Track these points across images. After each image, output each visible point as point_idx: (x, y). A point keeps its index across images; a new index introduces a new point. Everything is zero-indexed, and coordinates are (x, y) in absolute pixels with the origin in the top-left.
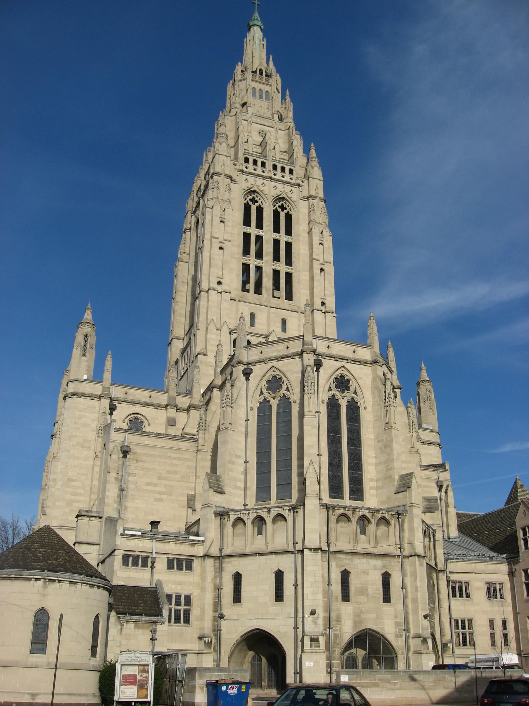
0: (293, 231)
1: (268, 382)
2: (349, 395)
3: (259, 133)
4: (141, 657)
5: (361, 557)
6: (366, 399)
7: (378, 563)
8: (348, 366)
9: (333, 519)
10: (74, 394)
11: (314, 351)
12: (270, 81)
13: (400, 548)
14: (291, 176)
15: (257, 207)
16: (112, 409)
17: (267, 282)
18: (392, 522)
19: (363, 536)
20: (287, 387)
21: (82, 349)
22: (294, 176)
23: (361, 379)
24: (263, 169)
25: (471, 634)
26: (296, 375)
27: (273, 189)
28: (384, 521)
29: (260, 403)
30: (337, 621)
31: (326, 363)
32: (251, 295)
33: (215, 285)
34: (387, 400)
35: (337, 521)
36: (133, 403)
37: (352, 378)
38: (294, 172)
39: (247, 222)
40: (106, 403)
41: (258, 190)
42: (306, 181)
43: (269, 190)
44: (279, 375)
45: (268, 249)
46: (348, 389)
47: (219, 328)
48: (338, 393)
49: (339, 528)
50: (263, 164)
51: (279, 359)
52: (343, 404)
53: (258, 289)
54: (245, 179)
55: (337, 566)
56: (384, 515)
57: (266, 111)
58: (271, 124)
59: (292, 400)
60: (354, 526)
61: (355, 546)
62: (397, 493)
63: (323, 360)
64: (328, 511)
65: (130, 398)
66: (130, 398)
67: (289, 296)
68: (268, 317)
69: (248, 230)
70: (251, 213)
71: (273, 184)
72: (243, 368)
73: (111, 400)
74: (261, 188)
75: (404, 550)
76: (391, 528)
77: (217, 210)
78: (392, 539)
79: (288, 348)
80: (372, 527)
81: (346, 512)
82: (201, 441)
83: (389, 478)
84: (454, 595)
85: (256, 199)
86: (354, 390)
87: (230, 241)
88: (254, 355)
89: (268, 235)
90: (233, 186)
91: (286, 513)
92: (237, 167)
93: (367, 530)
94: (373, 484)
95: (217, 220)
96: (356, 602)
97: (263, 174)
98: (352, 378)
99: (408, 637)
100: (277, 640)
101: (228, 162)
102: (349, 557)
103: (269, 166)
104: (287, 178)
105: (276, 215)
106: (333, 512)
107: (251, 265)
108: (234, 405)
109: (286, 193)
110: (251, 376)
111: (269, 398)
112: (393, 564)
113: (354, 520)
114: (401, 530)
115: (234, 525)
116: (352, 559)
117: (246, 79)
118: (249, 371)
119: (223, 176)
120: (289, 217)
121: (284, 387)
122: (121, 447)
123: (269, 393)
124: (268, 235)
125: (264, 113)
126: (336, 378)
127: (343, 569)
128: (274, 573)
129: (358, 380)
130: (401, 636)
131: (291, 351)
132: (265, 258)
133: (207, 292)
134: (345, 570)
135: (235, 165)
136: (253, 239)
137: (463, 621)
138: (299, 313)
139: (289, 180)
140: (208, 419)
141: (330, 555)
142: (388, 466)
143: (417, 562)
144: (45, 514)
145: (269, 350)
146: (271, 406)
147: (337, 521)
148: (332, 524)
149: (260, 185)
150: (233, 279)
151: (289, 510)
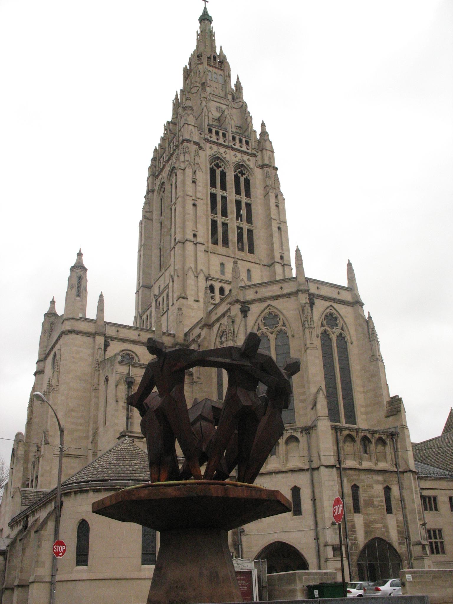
0: (252, 194)
1: (265, 318)
2: (338, 331)
3: (217, 109)
4: (242, 564)
5: (366, 473)
6: (351, 335)
7: (380, 478)
8: (336, 306)
9: (341, 439)
11: (105, 335)
12: (223, 66)
13: (396, 465)
15: (221, 172)
16: (106, 345)
17: (233, 237)
18: (388, 442)
19: (365, 455)
21: (82, 287)
23: (346, 317)
25: (442, 543)
26: (291, 312)
27: (233, 158)
28: (381, 441)
30: (351, 531)
31: (317, 302)
32: (220, 248)
33: (190, 237)
34: (371, 335)
35: (345, 441)
36: (123, 340)
37: (339, 316)
38: (250, 144)
39: (213, 184)
40: (100, 340)
41: (221, 157)
42: (260, 152)
43: (232, 158)
44: (275, 312)
45: (232, 207)
46: (336, 325)
47: (196, 275)
48: (329, 329)
49: (346, 447)
50: (224, 135)
52: (334, 338)
53: (226, 243)
55: (348, 481)
56: (380, 436)
57: (221, 91)
58: (226, 103)
60: (358, 445)
61: (360, 464)
62: (387, 417)
64: (336, 433)
65: (121, 335)
67: (251, 250)
69: (214, 191)
71: (233, 153)
72: (240, 307)
73: (106, 337)
74: (224, 155)
75: (399, 467)
76: (388, 448)
77: (189, 172)
78: (389, 457)
80: (372, 446)
81: (351, 433)
83: (379, 404)
84: (426, 509)
87: (202, 199)
88: (250, 295)
89: (232, 196)
90: (200, 152)
91: (298, 435)
92: (202, 136)
93: (368, 449)
94: (362, 410)
95: (189, 182)
96: (365, 514)
97: (225, 144)
98: (339, 316)
99: (410, 544)
100: (298, 551)
101: (196, 132)
102: (357, 473)
103: (229, 136)
104: (244, 149)
105: (237, 179)
106: (341, 433)
107: (218, 222)
108: (236, 339)
109: (245, 162)
110: (249, 314)
111: (268, 333)
112: (391, 479)
113: (358, 439)
114: (396, 450)
115: (287, 442)
116: (359, 475)
117: (202, 63)
118: (246, 309)
119: (192, 143)
120: (247, 181)
121: (281, 323)
122: (126, 379)
123: (267, 329)
124: (232, 196)
125: (219, 93)
126: (326, 316)
127: (353, 484)
128: (291, 489)
129: (344, 318)
130: (403, 544)
132: (230, 216)
133: (183, 243)
134: (355, 485)
135: (201, 134)
136: (219, 199)
137: (434, 532)
139: (246, 150)
141: (342, 472)
142: (376, 393)
143: (412, 476)
144: (47, 443)
145: (264, 290)
146: (269, 340)
147: (345, 441)
148: (341, 445)
150: (204, 232)
151: (302, 432)
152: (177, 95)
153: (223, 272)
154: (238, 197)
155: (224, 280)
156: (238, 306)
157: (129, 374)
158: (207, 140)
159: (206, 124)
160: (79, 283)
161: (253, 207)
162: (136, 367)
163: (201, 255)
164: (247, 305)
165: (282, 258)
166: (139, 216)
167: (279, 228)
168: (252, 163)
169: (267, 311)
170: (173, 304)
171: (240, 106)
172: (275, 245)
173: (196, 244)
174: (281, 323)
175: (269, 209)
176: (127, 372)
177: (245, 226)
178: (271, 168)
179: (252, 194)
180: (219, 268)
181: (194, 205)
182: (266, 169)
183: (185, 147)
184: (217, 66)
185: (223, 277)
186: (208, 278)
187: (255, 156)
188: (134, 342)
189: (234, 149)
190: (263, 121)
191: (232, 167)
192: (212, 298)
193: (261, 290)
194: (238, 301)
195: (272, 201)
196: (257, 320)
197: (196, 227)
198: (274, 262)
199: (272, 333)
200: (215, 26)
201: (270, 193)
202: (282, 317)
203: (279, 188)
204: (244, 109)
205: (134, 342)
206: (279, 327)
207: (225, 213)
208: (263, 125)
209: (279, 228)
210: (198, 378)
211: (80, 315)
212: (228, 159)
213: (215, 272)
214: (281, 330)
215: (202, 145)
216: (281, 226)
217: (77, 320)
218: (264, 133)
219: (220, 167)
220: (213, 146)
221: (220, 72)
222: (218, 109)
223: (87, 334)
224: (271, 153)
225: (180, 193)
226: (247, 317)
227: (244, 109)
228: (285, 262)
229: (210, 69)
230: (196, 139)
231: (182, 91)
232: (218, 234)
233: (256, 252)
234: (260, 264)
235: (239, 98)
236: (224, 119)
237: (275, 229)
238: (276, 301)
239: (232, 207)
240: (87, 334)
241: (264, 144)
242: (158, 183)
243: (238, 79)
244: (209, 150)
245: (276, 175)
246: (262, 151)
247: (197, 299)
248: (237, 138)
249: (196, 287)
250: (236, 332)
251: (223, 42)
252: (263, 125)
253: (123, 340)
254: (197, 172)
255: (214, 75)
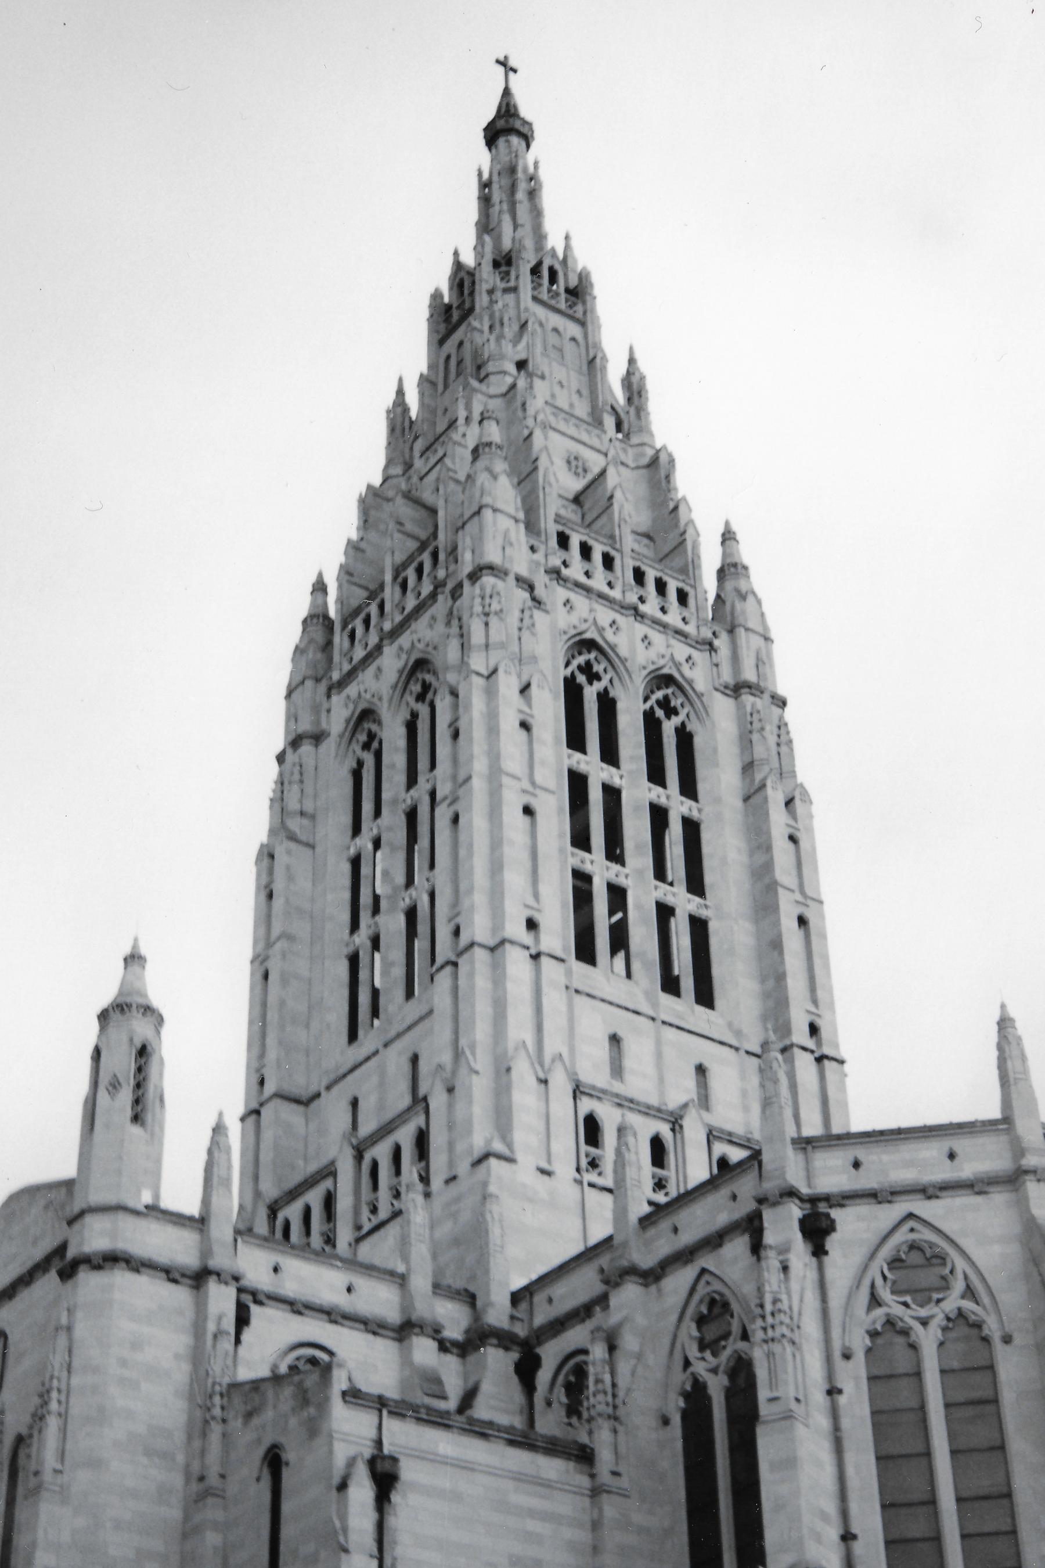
3: (569, 462)
10: (112, 1259)
14: (686, 614)
16: (242, 1319)
20: (968, 1287)
22: (690, 612)
24: (610, 576)
27: (640, 646)
29: (873, 1334)
33: (516, 929)
40: (222, 1300)
43: (640, 648)
44: (932, 1245)
45: (636, 829)
47: (542, 1076)
50: (608, 562)
51: (928, 1192)
54: (563, 600)
58: (595, 442)
59: (992, 1327)
63: (829, 1210)
66: (289, 1288)
67: (705, 996)
68: (659, 1055)
70: (585, 714)
73: (240, 1290)
79: (952, 1156)
82: (605, 1457)
85: (598, 668)
86: (740, 1331)
88: (831, 1174)
89: (638, 793)
90: (538, 614)
95: (509, 722)
101: (519, 535)
110: (832, 1242)
111: (907, 1319)
119: (511, 579)
123: (906, 1304)
124: (638, 793)
131: (967, 1169)
135: (532, 549)
138: (742, 1052)
140: (622, 1382)
145: (885, 1158)
149: (606, 625)
152: (400, 392)
153: (617, 1070)
154: (656, 794)
155: (631, 1101)
156: (795, 1211)
157: (379, 1443)
158: (555, 574)
159: (551, 517)
160: (139, 1070)
161: (706, 836)
162: (403, 1416)
163: (554, 1000)
164: (822, 1207)
165: (814, 1030)
166: (256, 826)
167: (802, 921)
168: (699, 675)
169: (902, 1236)
170: (452, 1179)
171: (645, 461)
172: (790, 982)
173: (536, 957)
174: (959, 1286)
175: (766, 847)
176: (373, 1433)
177: (684, 903)
178: (766, 696)
179: (702, 787)
180: (602, 1051)
181: (528, 811)
182: (748, 699)
183: (488, 591)
184: (563, 306)
185: (617, 1087)
186: (578, 1091)
187: (712, 648)
188: (332, 1315)
189: (639, 615)
190: (727, 524)
191: (639, 683)
192: (593, 1164)
193: (874, 1158)
194: (791, 1193)
195: (778, 820)
196: (865, 1268)
197: (536, 896)
198: (792, 1045)
199: (924, 1322)
200: (545, 155)
201: (769, 790)
202: (960, 1264)
203: (793, 774)
204: (663, 473)
205: (332, 1315)
206: (953, 1302)
207: (615, 852)
208: (728, 537)
209: (802, 921)
210: (615, 1474)
211: (147, 1198)
212: (623, 651)
213: (593, 1068)
214: (961, 1313)
215: (540, 591)
216: (809, 915)
217: (136, 1213)
218: (730, 570)
219: (598, 678)
220: (573, 596)
221: (573, 329)
222: (575, 464)
223: (170, 1274)
224: (761, 642)
225: (480, 766)
226: (826, 1253)
227: (663, 473)
228: (827, 1050)
229: (540, 312)
230: (524, 572)
231: (426, 382)
232: (594, 931)
233: (718, 1002)
234: (737, 1049)
235: (641, 430)
236: (604, 503)
237: (788, 924)
238: (934, 1203)
239: (636, 829)
240: (170, 1274)
241: (739, 606)
242: (339, 714)
243: (632, 361)
244: (567, 614)
245: (782, 725)
246: (731, 631)
247: (544, 1165)
248: (651, 575)
249: (540, 1125)
250: (796, 1309)
251: (571, 217)
252: (728, 537)
253: (297, 1307)
254: (534, 689)
255: (552, 339)
